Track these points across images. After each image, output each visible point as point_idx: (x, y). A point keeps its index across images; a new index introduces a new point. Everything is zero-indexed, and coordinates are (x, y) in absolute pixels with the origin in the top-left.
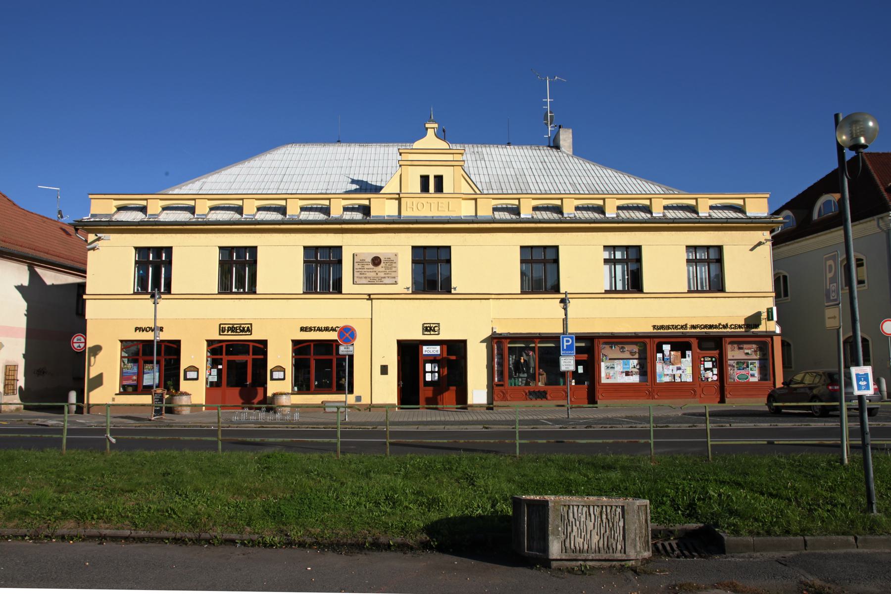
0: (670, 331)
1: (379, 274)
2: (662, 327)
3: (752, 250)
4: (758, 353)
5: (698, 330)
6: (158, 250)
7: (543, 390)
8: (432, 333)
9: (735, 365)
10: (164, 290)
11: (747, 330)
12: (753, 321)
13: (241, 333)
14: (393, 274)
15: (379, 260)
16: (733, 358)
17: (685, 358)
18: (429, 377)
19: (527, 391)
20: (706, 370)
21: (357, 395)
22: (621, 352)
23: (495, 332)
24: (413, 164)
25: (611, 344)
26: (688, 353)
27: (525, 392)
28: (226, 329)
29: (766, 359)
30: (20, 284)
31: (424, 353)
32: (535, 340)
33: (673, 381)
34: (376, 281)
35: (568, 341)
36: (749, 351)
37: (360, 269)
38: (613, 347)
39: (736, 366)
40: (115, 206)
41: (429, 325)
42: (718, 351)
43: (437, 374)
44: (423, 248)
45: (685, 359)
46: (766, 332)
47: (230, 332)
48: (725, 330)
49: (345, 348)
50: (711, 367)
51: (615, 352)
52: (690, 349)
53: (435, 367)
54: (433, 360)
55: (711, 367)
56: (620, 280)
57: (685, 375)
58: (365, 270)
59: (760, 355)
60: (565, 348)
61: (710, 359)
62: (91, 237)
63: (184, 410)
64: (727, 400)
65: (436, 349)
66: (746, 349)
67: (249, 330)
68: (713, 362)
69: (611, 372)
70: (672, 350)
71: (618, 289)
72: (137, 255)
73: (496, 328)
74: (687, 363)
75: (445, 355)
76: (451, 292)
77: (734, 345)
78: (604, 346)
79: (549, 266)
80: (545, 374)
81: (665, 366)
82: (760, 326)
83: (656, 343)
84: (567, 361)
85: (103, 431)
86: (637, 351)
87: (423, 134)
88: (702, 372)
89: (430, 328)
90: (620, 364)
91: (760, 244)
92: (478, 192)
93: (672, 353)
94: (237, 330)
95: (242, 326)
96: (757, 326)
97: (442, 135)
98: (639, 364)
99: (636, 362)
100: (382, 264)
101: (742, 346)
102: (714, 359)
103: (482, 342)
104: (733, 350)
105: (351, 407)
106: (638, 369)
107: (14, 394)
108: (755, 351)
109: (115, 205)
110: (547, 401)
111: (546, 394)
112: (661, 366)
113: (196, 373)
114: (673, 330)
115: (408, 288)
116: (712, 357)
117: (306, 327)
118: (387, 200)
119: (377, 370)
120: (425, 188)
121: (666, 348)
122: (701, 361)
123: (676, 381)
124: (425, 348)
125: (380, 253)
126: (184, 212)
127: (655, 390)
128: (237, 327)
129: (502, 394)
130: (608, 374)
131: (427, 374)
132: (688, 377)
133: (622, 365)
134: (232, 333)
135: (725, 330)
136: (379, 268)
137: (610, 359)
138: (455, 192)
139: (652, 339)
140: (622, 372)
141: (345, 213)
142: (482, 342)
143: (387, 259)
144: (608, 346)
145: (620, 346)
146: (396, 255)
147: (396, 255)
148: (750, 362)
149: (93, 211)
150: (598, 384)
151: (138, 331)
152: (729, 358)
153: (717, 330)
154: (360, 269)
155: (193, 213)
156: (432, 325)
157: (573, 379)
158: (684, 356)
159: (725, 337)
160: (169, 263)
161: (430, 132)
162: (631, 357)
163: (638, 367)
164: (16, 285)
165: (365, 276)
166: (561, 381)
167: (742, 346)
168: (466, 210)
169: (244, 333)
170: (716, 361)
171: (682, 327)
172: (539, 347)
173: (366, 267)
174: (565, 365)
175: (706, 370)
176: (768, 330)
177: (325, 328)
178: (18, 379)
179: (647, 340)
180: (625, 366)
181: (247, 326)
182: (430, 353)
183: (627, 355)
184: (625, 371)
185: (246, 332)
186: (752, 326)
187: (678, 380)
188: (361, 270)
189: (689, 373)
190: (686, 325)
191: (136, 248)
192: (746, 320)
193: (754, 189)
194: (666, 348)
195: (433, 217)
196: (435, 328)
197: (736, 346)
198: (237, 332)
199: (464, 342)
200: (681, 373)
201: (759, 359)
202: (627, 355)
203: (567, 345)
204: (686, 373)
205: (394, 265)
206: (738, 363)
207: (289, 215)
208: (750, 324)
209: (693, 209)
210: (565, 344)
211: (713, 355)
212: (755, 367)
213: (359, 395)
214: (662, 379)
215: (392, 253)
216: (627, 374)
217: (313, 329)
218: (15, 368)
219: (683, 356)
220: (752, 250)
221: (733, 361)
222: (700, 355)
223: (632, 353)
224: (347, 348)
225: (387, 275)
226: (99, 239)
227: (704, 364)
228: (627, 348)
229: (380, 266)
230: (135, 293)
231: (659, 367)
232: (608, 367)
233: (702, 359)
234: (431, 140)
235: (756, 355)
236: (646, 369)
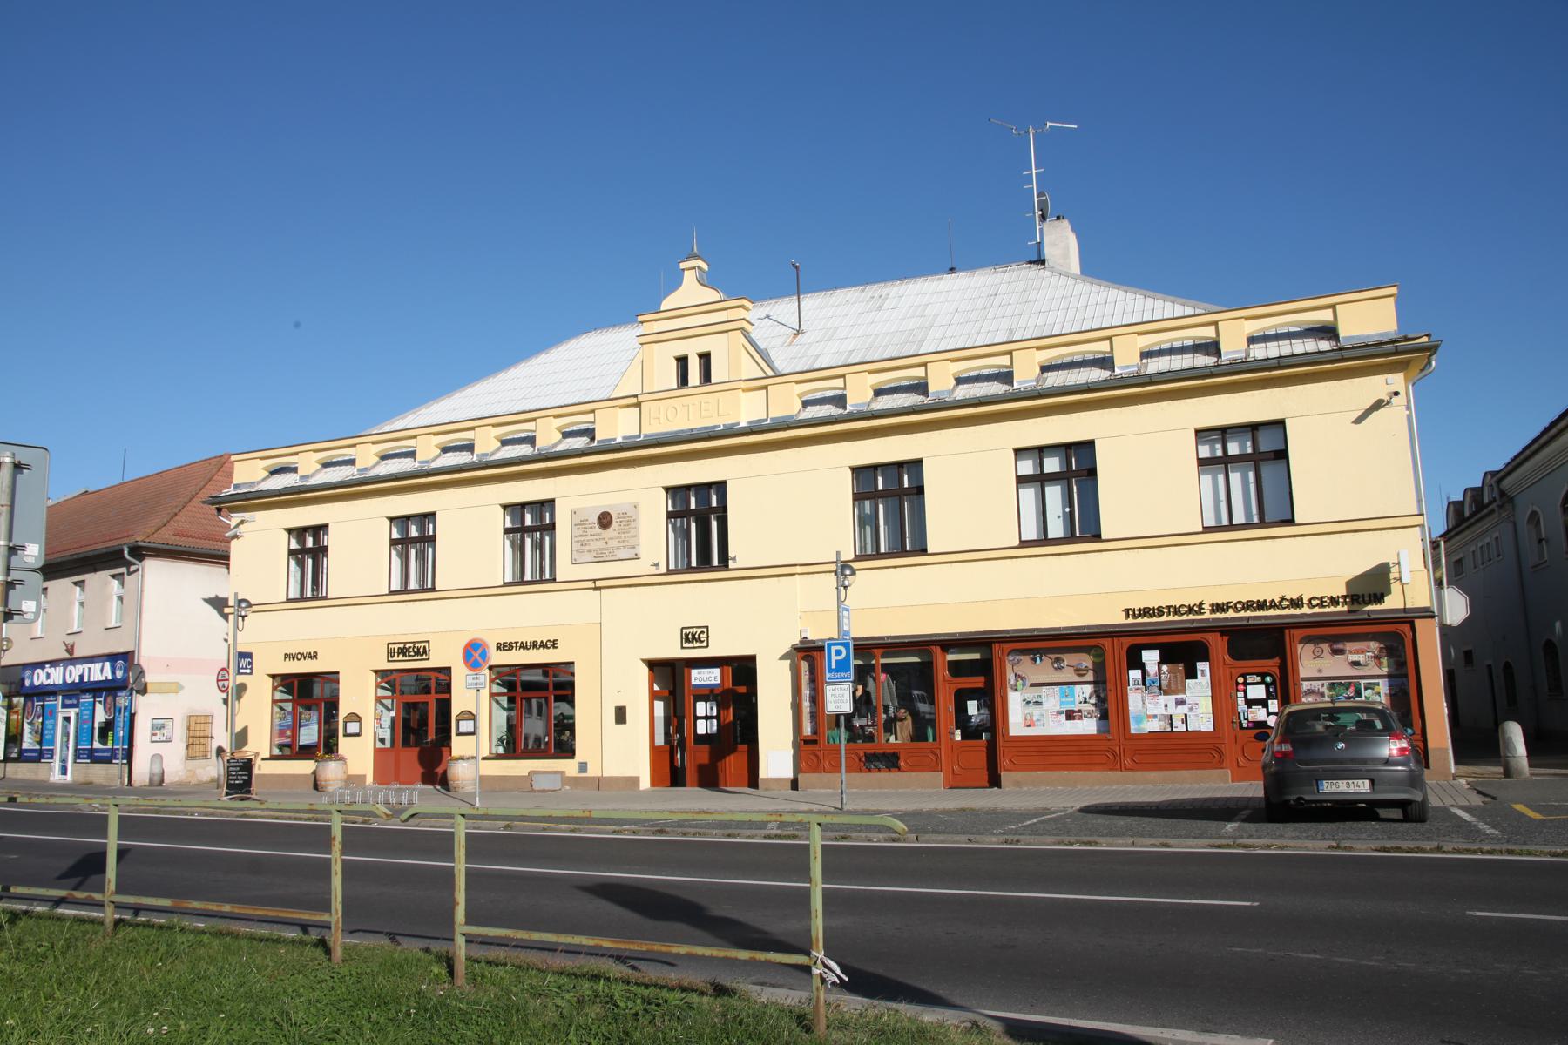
0: (1164, 618)
1: (610, 542)
2: (1145, 612)
3: (1358, 421)
4: (1385, 661)
5: (1231, 614)
6: (703, 489)
7: (892, 751)
8: (698, 644)
9: (1325, 690)
10: (719, 563)
11: (1355, 607)
12: (1373, 584)
13: (416, 658)
14: (632, 542)
15: (609, 518)
16: (1321, 675)
17: (1195, 677)
18: (701, 728)
19: (861, 754)
20: (1250, 703)
21: (581, 761)
22: (1055, 668)
23: (805, 638)
24: (660, 339)
25: (1034, 653)
26: (1203, 666)
27: (857, 754)
28: (396, 651)
29: (1406, 676)
30: (213, 596)
31: (693, 682)
32: (875, 650)
33: (1169, 729)
34: (604, 555)
35: (838, 653)
36: (1360, 658)
37: (581, 536)
38: (1038, 659)
39: (1327, 693)
40: (436, 446)
41: (691, 630)
42: (1277, 660)
43: (715, 721)
44: (1064, 448)
45: (1194, 681)
46: (1405, 610)
47: (401, 656)
48: (1298, 611)
49: (473, 679)
50: (1263, 696)
51: (1042, 669)
52: (1205, 658)
53: (712, 709)
54: (706, 694)
55: (1263, 696)
56: (1059, 517)
57: (1196, 715)
58: (589, 538)
59: (1388, 667)
60: (833, 666)
61: (1259, 679)
62: (236, 518)
63: (331, 785)
64: (1004, 775)
65: (714, 675)
66: (1351, 652)
67: (423, 652)
68: (1267, 686)
69: (1035, 712)
70: (1163, 661)
71: (1050, 536)
72: (670, 501)
73: (806, 631)
74: (1199, 690)
75: (729, 684)
76: (727, 566)
77: (1322, 645)
78: (1018, 657)
79: (1268, 470)
80: (909, 717)
81: (1149, 698)
82: (1386, 598)
83: (1125, 649)
84: (837, 693)
85: (805, 827)
86: (1091, 666)
87: (675, 282)
88: (1242, 708)
89: (693, 635)
90: (1053, 695)
91: (1378, 405)
92: (770, 373)
93: (1165, 668)
94: (410, 652)
95: (417, 645)
96: (1379, 598)
97: (706, 281)
98: (1096, 693)
99: (1088, 689)
100: (614, 525)
101: (1340, 646)
102: (1268, 679)
103: (782, 658)
104: (1318, 657)
105: (575, 781)
106: (1092, 704)
107: (205, 757)
108: (1377, 658)
109: (438, 442)
110: (900, 774)
111: (898, 758)
112: (1139, 696)
113: (472, 722)
114: (1171, 618)
115: (657, 565)
116: (1263, 675)
117: (504, 643)
118: (1039, 352)
119: (610, 715)
120: (683, 380)
121: (1151, 657)
122: (1238, 684)
123: (1175, 730)
124: (695, 673)
125: (609, 506)
126: (986, 384)
127: (1005, 753)
128: (410, 647)
129: (815, 760)
130: (1028, 717)
131: (699, 722)
132: (1202, 721)
133: (1058, 697)
134: (405, 658)
135: (1298, 611)
136: (610, 532)
137: (1032, 685)
138: (644, 392)
139: (1116, 640)
140: (1062, 712)
141: (1251, 346)
142: (782, 658)
143: (622, 515)
144: (1027, 657)
145: (1053, 656)
146: (635, 507)
147: (635, 507)
148: (1363, 682)
149: (236, 481)
150: (1001, 738)
151: (287, 659)
152: (1302, 676)
153: (1278, 612)
154: (581, 536)
155: (534, 446)
156: (695, 630)
157: (957, 729)
158: (1191, 674)
159: (1287, 628)
160: (722, 513)
161: (689, 278)
162: (1077, 679)
163: (1093, 700)
164: (206, 597)
165: (588, 547)
166: (930, 731)
167: (1340, 646)
168: (747, 409)
169: (419, 658)
170: (1273, 683)
171: (1191, 610)
172: (882, 664)
173: (590, 531)
174: (835, 701)
175: (1250, 703)
176: (1407, 606)
177: (1140, 610)
178: (213, 735)
179: (1106, 642)
180: (1063, 700)
181: (423, 645)
182: (703, 683)
183: (1069, 676)
184: (1065, 710)
185: (422, 655)
186: (1367, 599)
187: (1179, 727)
188: (580, 539)
189: (1203, 710)
190: (1201, 604)
191: (667, 489)
192: (1349, 584)
193: (1359, 281)
194: (1151, 657)
195: (692, 430)
196: (702, 635)
197: (1325, 646)
198: (409, 656)
199: (752, 659)
200: (1186, 711)
201: (1389, 676)
202: (1069, 676)
203: (836, 661)
204: (1198, 711)
205: (633, 524)
206: (1332, 687)
207: (852, 406)
208: (1360, 594)
209: (1213, 348)
210: (834, 658)
211: (1266, 670)
212: (1379, 694)
213: (584, 761)
214: (1142, 726)
215: (630, 504)
216: (1070, 715)
217: (1165, 610)
218: (207, 719)
219: (1191, 674)
220: (1358, 421)
221: (1320, 683)
222: (1234, 671)
223: (1079, 671)
224: (477, 678)
225: (622, 544)
226: (242, 522)
227: (1245, 692)
228: (1069, 659)
229: (611, 529)
230: (672, 570)
231: (1135, 699)
232: (1028, 702)
233: (1241, 680)
234: (691, 291)
235: (1380, 665)
236: (1110, 706)
